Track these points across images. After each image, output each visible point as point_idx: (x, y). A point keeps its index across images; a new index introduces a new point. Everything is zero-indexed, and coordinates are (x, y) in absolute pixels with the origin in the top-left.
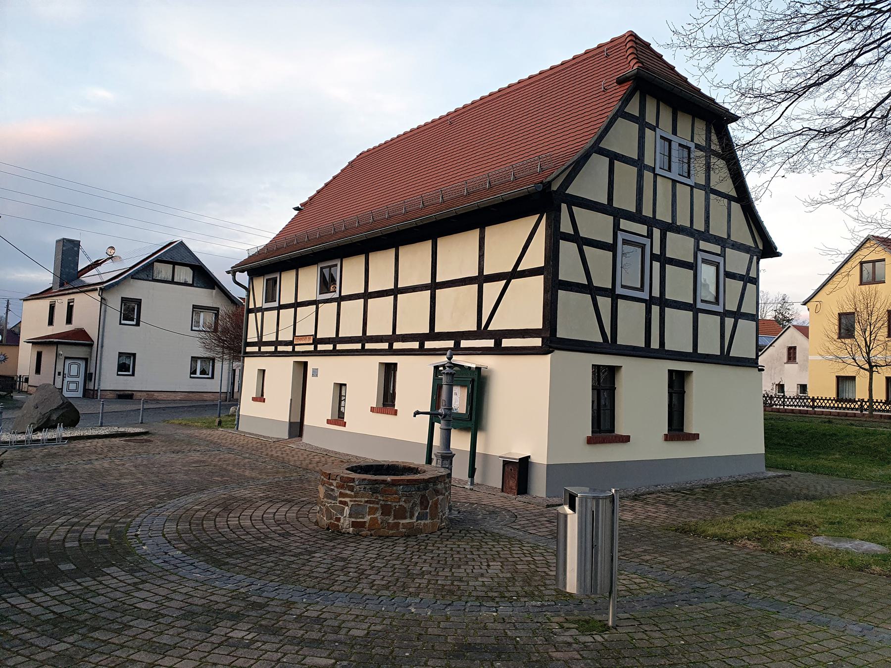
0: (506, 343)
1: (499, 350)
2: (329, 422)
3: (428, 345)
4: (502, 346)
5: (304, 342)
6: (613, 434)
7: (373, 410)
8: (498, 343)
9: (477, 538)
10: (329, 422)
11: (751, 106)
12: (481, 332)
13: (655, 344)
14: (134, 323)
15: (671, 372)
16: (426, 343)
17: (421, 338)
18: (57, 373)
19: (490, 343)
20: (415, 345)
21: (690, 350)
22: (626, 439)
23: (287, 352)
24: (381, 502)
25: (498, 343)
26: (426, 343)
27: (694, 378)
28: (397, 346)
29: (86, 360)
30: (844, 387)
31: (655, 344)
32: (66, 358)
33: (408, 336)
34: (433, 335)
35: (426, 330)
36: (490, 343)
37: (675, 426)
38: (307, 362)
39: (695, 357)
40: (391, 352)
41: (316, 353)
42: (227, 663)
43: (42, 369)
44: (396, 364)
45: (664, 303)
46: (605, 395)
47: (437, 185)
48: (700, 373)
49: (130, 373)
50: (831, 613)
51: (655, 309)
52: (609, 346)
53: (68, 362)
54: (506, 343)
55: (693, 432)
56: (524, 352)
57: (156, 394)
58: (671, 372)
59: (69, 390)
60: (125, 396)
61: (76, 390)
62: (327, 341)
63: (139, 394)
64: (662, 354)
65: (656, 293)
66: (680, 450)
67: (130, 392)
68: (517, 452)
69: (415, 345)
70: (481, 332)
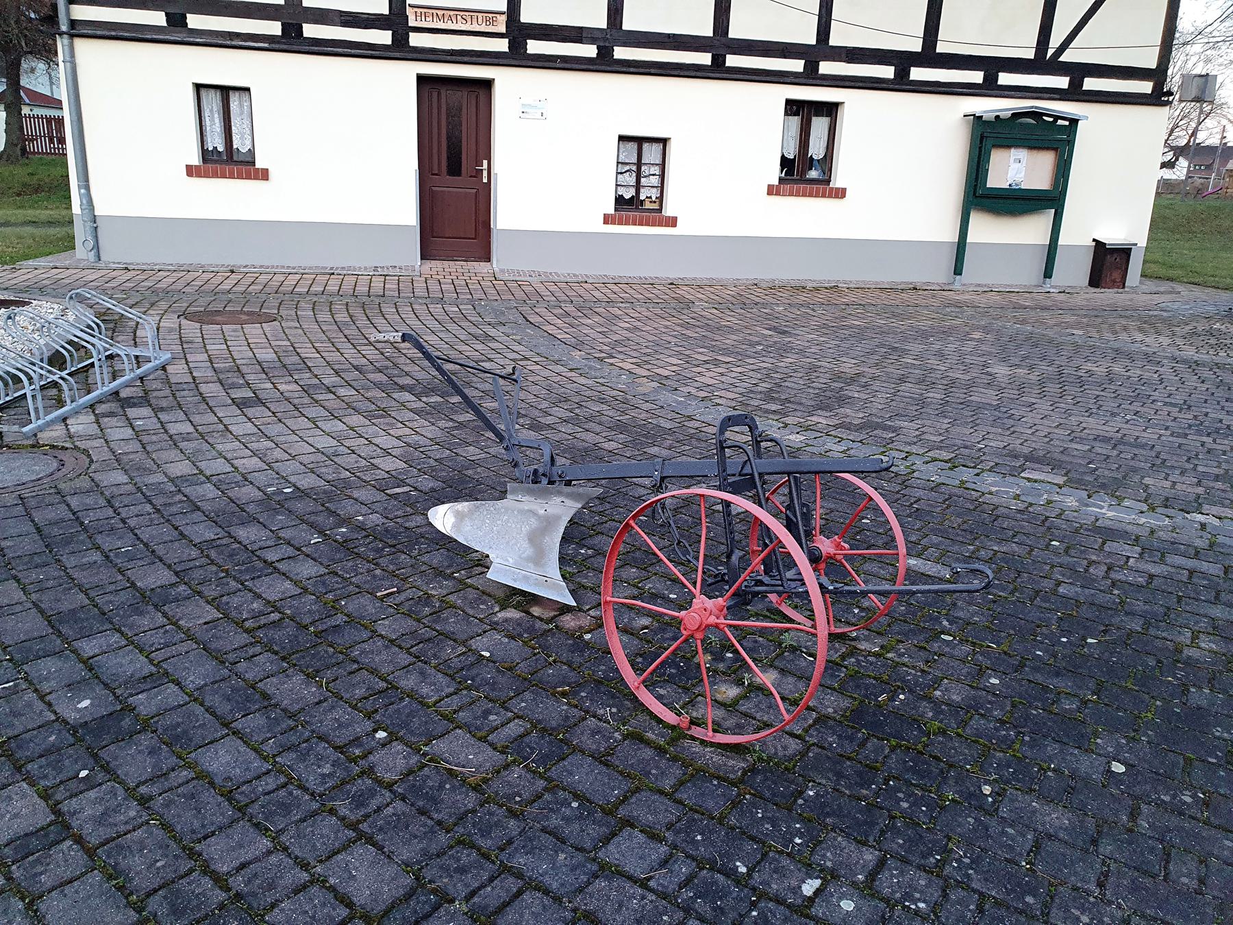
0: (1090, 84)
1: (1075, 93)
2: (607, 219)
3: (917, 74)
6: (482, 267)
8: (1076, 84)
10: (607, 219)
12: (1041, 63)
17: (903, 61)
19: (1062, 82)
20: (887, 72)
25: (1076, 84)
27: (847, 120)
28: (826, 68)
33: (619, 18)
34: (929, 57)
35: (916, 46)
36: (1062, 82)
40: (811, 76)
41: (517, 57)
50: (1050, 480)
54: (1090, 84)
56: (1110, 99)
58: (422, 80)
62: (574, 33)
68: (1113, 236)
69: (887, 72)
70: (1041, 63)
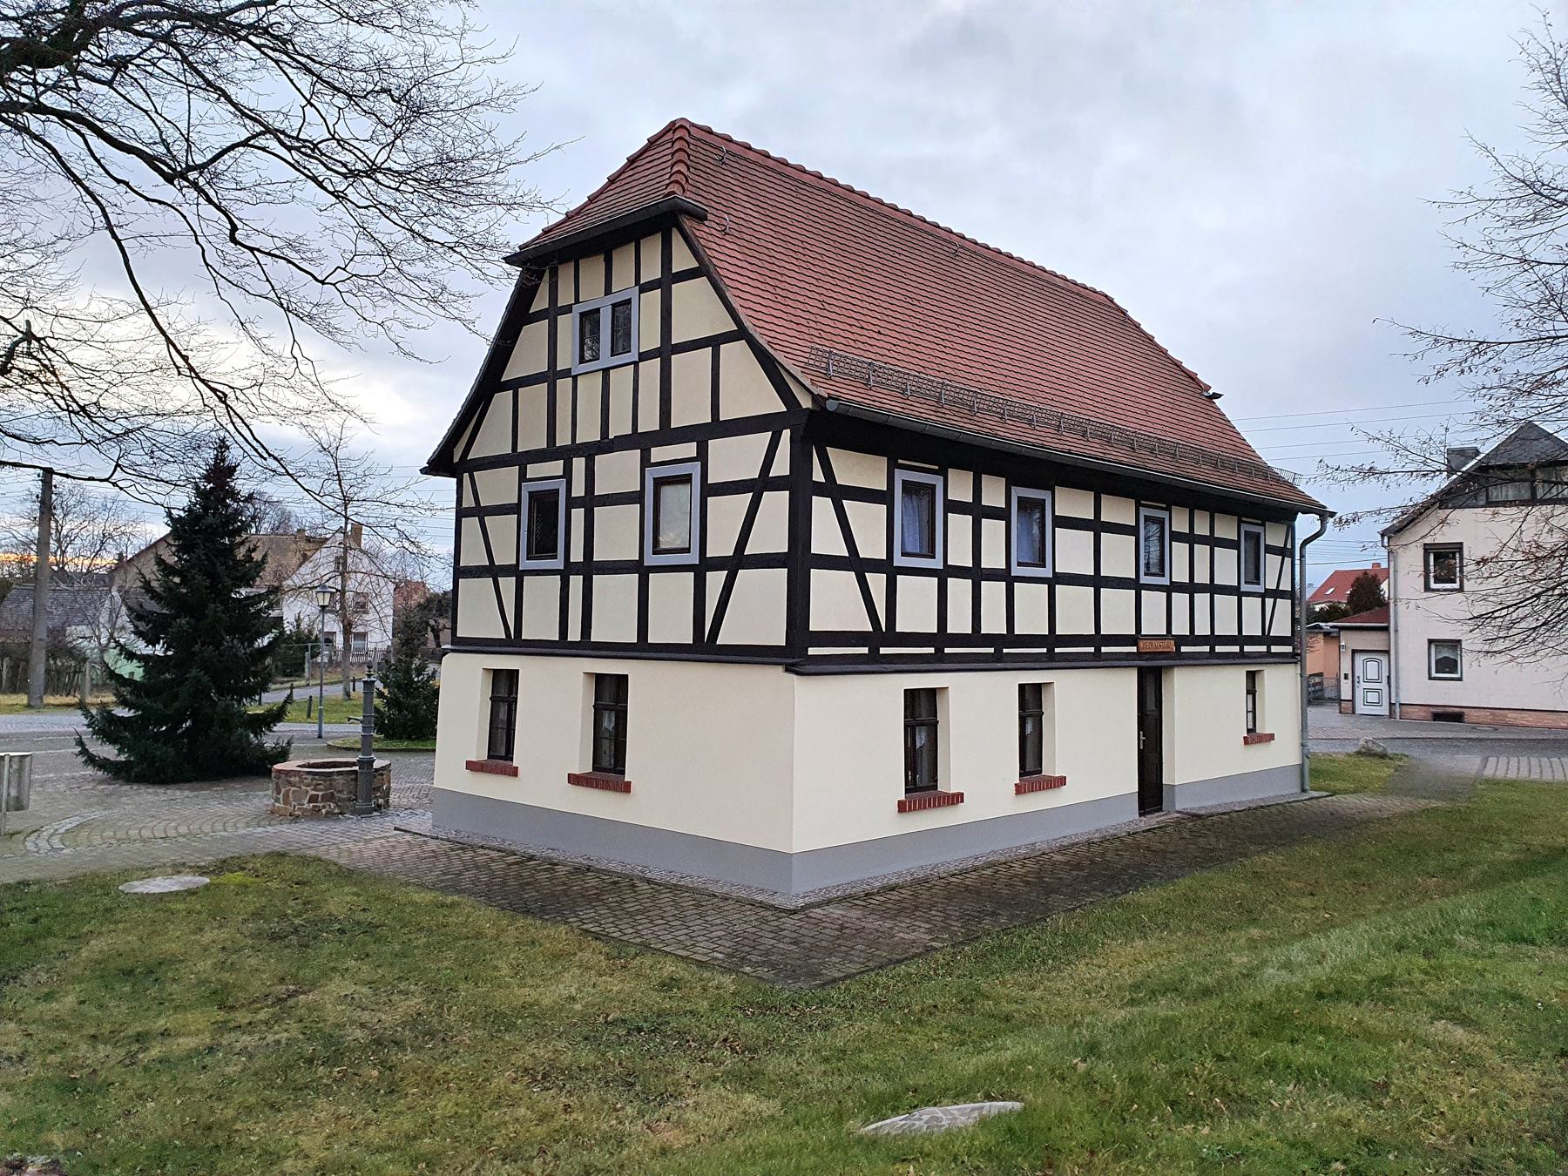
4: (718, 643)
9: (655, 913)
11: (227, 391)
13: (574, 634)
14: (1456, 586)
18: (1350, 676)
21: (633, 638)
22: (957, 798)
27: (1265, 672)
29: (1387, 652)
31: (574, 634)
32: (1354, 652)
37: (607, 761)
39: (643, 649)
44: (518, 671)
45: (590, 568)
46: (504, 709)
47: (1006, 348)
48: (639, 674)
49: (1434, 674)
51: (576, 582)
52: (514, 643)
53: (1360, 659)
55: (953, 791)
57: (1510, 714)
59: (1367, 703)
60: (1451, 716)
61: (1378, 704)
63: (1474, 713)
64: (587, 647)
65: (577, 556)
67: (1457, 710)
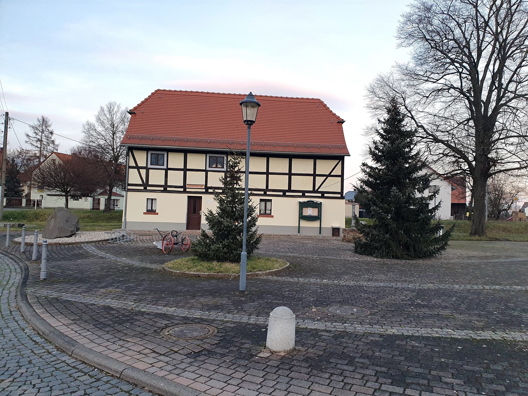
1: (323, 197)
3: (287, 194)
5: (192, 187)
7: (144, 213)
15: (188, 196)
16: (325, 194)
17: (284, 192)
19: (320, 195)
23: (262, 194)
24: (410, 253)
26: (325, 194)
30: (191, 200)
34: (290, 190)
36: (320, 195)
38: (260, 199)
42: (245, 364)
43: (49, 196)
54: (326, 195)
58: (188, 196)
66: (151, 218)
70: (314, 191)
